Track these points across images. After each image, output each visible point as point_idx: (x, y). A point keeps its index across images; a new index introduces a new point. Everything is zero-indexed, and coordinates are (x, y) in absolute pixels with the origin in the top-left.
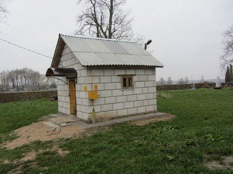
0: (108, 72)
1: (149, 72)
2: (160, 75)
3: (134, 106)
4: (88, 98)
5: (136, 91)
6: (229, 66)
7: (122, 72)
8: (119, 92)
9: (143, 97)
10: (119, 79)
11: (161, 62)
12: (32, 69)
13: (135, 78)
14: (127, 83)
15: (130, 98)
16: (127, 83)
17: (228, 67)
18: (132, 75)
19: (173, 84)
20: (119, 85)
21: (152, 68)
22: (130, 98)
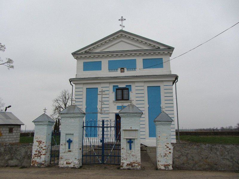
0: (6, 127)
1: (18, 127)
2: (23, 128)
3: (122, 92)
4: (132, 101)
5: (14, 134)
6: (58, 121)
7: (10, 127)
8: (8, 134)
9: (15, 136)
10: (8, 129)
11: (23, 122)
12: (232, 126)
13: (14, 129)
14: (11, 131)
15: (11, 137)
16: (11, 131)
17: (57, 120)
18: (13, 128)
19: (23, 132)
20: (8, 132)
21: (20, 125)
22: (11, 137)
